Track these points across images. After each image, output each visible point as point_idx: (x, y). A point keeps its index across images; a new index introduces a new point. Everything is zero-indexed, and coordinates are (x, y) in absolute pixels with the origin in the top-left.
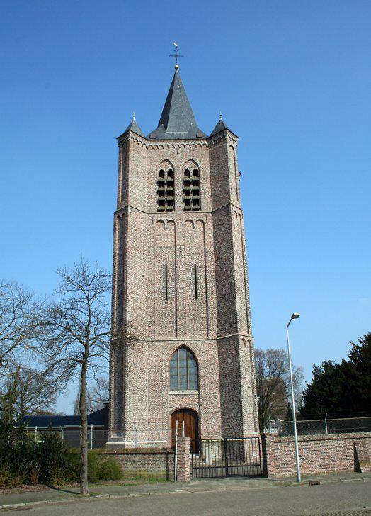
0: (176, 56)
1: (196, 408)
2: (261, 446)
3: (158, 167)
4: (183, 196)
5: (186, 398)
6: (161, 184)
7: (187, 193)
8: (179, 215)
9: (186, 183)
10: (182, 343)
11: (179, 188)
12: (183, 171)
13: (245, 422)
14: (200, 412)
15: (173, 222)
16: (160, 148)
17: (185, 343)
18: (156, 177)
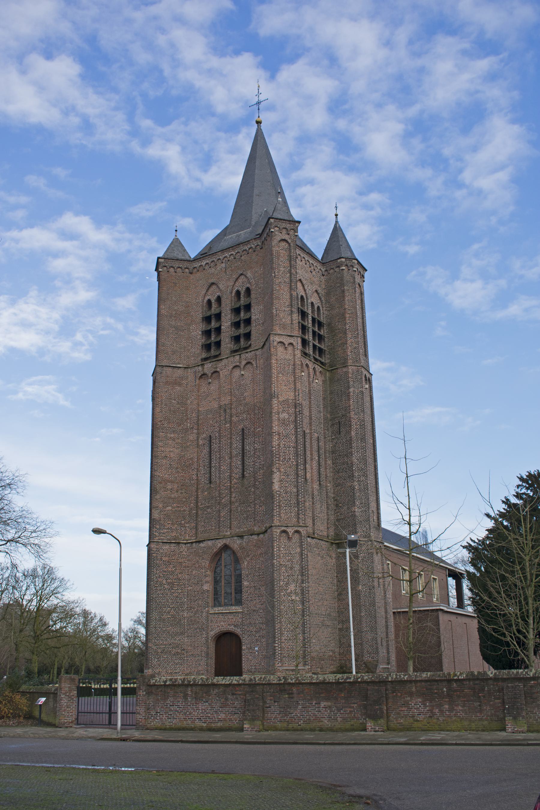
1: (238, 631)
5: (224, 619)
11: (226, 323)
17: (227, 541)
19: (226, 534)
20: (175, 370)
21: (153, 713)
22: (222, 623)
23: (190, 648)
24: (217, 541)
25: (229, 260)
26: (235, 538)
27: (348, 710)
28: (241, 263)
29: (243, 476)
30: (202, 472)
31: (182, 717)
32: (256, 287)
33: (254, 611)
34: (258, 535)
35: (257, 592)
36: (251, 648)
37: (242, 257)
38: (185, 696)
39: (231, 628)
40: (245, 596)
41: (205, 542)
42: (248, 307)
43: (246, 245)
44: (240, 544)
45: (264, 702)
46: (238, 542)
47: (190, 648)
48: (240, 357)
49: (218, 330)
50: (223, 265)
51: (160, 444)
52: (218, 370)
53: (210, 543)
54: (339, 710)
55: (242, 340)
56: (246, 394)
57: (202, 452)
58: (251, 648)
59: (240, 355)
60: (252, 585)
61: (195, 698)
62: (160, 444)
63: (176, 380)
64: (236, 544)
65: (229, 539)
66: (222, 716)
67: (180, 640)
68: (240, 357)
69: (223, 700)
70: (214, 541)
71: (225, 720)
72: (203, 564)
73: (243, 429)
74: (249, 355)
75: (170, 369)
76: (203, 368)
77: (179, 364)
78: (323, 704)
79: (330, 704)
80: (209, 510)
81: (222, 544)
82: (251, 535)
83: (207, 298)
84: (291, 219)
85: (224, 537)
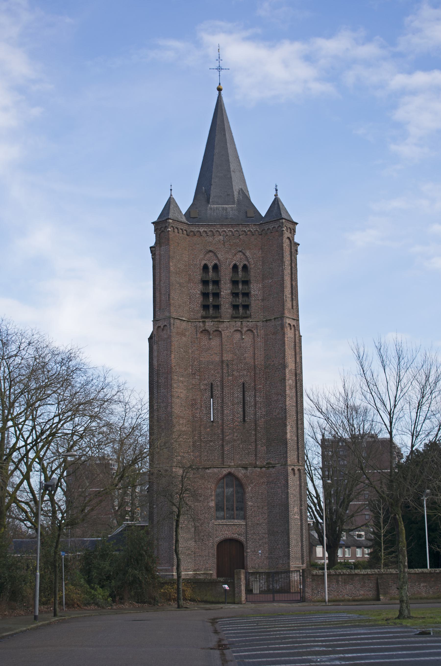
0: (219, 69)
1: (242, 539)
2: (301, 577)
3: (201, 260)
4: (230, 299)
5: (231, 528)
6: (205, 283)
7: (235, 295)
8: (228, 327)
9: (235, 283)
10: (229, 470)
11: (226, 290)
12: (231, 266)
13: (292, 554)
14: (247, 543)
15: (211, 251)
16: (204, 235)
17: (233, 470)
18: (198, 275)
19: (230, 464)
20: (182, 322)
21: (316, 592)
22: (227, 532)
23: (197, 550)
24: (223, 469)
25: (227, 235)
26: (240, 468)
27: (436, 587)
28: (240, 241)
29: (244, 420)
30: (204, 412)
31: (336, 594)
32: (254, 267)
33: (258, 524)
34: (261, 468)
35: (260, 510)
36: (255, 551)
37: (241, 237)
38: (338, 582)
39: (236, 536)
40: (249, 513)
41: (211, 469)
42: (246, 283)
43: (246, 227)
44: (245, 473)
45: (388, 584)
46: (243, 471)
47: (197, 550)
48: (242, 324)
49: (217, 295)
50: (221, 237)
51: (175, 385)
52: (220, 329)
53: (216, 470)
54: (431, 587)
55: (241, 309)
56: (246, 355)
57: (203, 395)
58: (255, 551)
59: (241, 322)
60: (256, 504)
61: (344, 582)
62: (175, 385)
63: (182, 331)
64: (240, 473)
65: (234, 469)
66: (362, 592)
67: (190, 544)
68: (242, 324)
69: (362, 583)
70: (219, 469)
71: (364, 595)
72: (209, 486)
73: (243, 384)
74: (250, 324)
75: (178, 321)
76: (205, 325)
77: (183, 317)
78: (422, 585)
79: (426, 584)
80: (211, 444)
81: (227, 471)
82: (255, 468)
83: (203, 262)
84: (289, 219)
85: (230, 467)
